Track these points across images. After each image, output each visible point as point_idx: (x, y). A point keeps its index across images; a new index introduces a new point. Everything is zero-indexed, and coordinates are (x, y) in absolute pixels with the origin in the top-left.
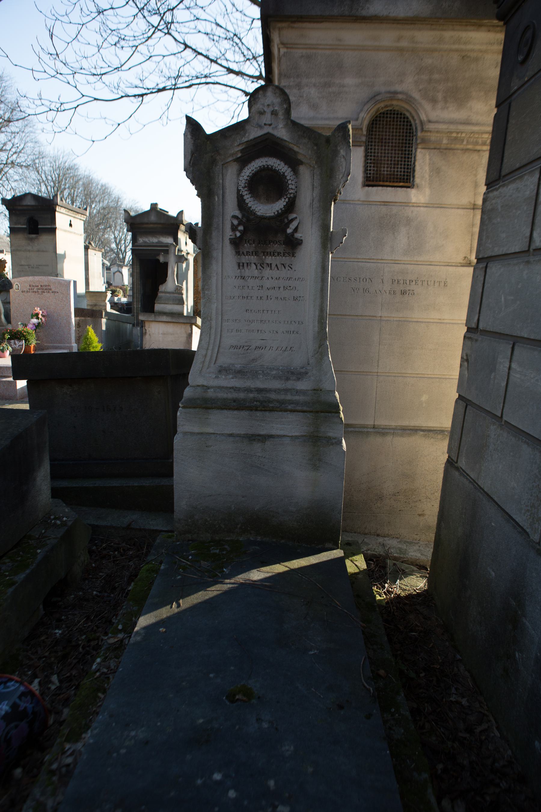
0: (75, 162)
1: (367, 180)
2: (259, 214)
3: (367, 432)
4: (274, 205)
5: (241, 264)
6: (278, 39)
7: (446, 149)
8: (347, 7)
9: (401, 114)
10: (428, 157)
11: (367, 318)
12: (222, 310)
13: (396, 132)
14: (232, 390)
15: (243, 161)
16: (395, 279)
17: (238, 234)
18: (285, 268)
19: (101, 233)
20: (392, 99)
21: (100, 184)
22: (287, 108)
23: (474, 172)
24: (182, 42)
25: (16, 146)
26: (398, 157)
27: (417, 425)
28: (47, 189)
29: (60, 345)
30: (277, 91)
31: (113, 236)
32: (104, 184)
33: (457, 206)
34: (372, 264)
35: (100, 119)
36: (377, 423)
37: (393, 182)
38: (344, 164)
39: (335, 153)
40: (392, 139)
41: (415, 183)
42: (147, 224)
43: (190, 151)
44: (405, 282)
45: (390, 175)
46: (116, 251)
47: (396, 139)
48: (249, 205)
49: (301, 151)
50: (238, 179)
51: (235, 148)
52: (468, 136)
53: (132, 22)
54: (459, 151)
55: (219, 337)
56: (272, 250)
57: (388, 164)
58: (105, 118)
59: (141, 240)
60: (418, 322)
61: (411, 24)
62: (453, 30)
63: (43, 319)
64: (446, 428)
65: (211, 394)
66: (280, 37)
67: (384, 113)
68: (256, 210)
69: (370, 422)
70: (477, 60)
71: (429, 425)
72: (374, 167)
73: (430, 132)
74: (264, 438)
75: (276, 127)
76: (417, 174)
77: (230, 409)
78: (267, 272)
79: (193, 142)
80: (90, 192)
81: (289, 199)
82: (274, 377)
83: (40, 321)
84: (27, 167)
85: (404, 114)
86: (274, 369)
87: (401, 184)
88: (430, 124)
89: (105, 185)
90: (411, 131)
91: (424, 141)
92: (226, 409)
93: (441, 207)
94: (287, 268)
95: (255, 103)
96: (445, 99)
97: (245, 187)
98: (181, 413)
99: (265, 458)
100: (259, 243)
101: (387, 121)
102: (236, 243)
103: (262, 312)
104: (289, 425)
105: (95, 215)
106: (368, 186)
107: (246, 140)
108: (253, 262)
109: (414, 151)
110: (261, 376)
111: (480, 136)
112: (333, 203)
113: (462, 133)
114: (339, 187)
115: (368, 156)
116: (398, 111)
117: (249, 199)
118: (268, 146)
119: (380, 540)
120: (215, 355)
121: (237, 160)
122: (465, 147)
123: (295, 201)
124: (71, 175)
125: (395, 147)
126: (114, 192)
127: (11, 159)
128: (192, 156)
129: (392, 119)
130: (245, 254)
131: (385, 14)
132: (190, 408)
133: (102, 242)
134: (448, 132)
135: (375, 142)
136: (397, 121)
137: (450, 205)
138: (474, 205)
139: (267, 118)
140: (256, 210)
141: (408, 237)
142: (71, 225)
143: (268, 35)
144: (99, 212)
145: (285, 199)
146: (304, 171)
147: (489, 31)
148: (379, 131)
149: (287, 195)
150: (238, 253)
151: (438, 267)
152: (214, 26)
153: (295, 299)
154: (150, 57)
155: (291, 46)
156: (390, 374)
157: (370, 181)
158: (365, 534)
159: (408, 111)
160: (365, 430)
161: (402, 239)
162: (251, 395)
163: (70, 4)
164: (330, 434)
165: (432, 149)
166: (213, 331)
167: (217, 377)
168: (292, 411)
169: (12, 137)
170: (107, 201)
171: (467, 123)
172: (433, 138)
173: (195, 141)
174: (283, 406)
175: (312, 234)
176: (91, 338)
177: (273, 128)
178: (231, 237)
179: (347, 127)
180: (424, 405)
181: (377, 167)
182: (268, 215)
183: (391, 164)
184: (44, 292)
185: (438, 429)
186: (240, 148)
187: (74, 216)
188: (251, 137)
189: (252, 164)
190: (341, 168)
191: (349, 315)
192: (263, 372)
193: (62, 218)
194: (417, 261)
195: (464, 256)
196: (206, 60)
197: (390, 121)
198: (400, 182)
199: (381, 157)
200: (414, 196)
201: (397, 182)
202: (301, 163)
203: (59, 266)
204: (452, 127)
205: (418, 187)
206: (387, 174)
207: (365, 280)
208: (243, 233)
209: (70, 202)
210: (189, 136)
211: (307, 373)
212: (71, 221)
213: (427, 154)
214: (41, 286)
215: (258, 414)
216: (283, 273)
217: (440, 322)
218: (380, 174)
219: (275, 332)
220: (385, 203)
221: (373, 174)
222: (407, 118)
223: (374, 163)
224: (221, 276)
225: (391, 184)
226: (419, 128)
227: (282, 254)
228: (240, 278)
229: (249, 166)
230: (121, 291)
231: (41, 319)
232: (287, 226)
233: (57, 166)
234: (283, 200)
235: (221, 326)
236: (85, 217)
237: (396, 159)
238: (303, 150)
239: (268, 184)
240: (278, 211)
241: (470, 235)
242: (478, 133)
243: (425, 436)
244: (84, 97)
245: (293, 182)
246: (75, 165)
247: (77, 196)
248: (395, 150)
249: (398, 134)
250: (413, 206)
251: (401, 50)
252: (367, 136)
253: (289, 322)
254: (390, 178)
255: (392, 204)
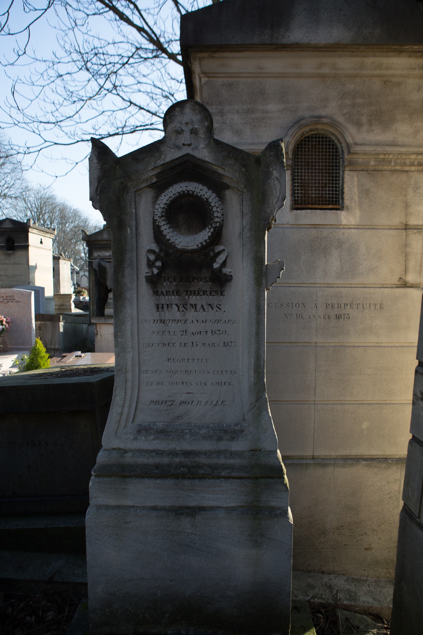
0: (53, 193)
1: (295, 204)
2: (179, 247)
3: (307, 464)
4: (198, 236)
5: (160, 306)
6: (199, 69)
7: (374, 171)
8: (267, 35)
9: (326, 138)
10: (356, 179)
11: (301, 344)
12: (139, 360)
13: (322, 155)
14: (154, 454)
15: (159, 188)
16: (329, 303)
17: (156, 271)
18: (212, 309)
19: (73, 246)
20: (316, 123)
21: (72, 209)
22: (208, 126)
23: (404, 193)
24: (128, 100)
25: (8, 183)
26: (326, 180)
27: (359, 454)
28: (32, 214)
29: (22, 347)
30: (197, 107)
31: (82, 248)
32: (75, 209)
33: (388, 227)
34: (304, 289)
35: (62, 159)
36: (316, 454)
37: (322, 204)
38: (278, 186)
39: (268, 175)
40: (319, 162)
41: (344, 205)
42: (101, 241)
43: (96, 177)
44: (339, 306)
45: (319, 197)
46: (85, 259)
47: (322, 162)
48: (168, 237)
49: (226, 174)
50: (154, 208)
51: (149, 172)
52: (395, 157)
53: (87, 85)
54: (387, 172)
55: (136, 391)
56: (196, 289)
57: (315, 187)
58: (66, 159)
59: (96, 254)
60: (354, 346)
61: (332, 51)
62: (374, 56)
63: (7, 326)
64: (389, 455)
65: (129, 459)
66: (200, 66)
67: (309, 137)
68: (176, 242)
69: (309, 453)
70: (399, 84)
71: (371, 454)
72: (301, 190)
73: (357, 154)
74: (193, 511)
75: (196, 147)
76: (346, 196)
77: (151, 477)
78: (191, 314)
79: (99, 167)
80: (65, 215)
81: (215, 228)
82: (204, 437)
83: (4, 327)
84: (16, 198)
85: (330, 138)
86: (203, 426)
87: (331, 206)
88: (357, 146)
89: (76, 210)
90: (338, 154)
91: (351, 163)
92: (148, 477)
93: (372, 229)
94: (215, 309)
95: (171, 122)
96: (370, 123)
97: (162, 216)
98: (93, 483)
99: (195, 534)
100: (181, 281)
101: (312, 145)
102: (153, 281)
103: (186, 361)
104: (223, 495)
105: (69, 232)
106: (297, 209)
107: (162, 163)
108: (174, 303)
109: (341, 173)
110: (188, 436)
111: (407, 157)
112: (267, 231)
113: (389, 154)
114: (273, 214)
115: (295, 179)
116: (323, 134)
117: (167, 231)
118: (188, 168)
119: (326, 579)
120: (133, 413)
121: (152, 186)
122: (393, 168)
123: (222, 230)
124: (51, 203)
125: (322, 169)
126: (83, 215)
127: (4, 193)
128: (99, 183)
129: (317, 143)
130: (165, 294)
131: (306, 42)
132: (104, 476)
133: (74, 253)
134: (376, 154)
135: (301, 165)
136: (322, 145)
137: (381, 226)
138: (406, 225)
139: (186, 138)
140: (176, 242)
141: (341, 260)
142: (41, 242)
143: (189, 68)
144: (71, 230)
145: (210, 229)
146: (232, 198)
147: (410, 56)
148: (305, 155)
149: (212, 224)
150: (156, 293)
151: (373, 289)
152: (153, 87)
153: (225, 345)
154: (103, 112)
155: (212, 75)
156: (328, 402)
157: (298, 204)
158: (309, 572)
159: (333, 134)
160: (304, 462)
161: (334, 262)
162: (177, 460)
163: (37, 74)
164: (274, 504)
165: (360, 171)
166: (129, 384)
167: (135, 439)
168: (226, 478)
169: (5, 176)
170: (77, 222)
171: (393, 144)
172: (360, 160)
173: (101, 166)
174: (215, 472)
175: (243, 269)
176: (38, 349)
177: (193, 149)
178: (148, 275)
179: (279, 145)
180: (365, 432)
181: (305, 190)
182: (190, 248)
183: (319, 187)
184: (9, 302)
185: (381, 457)
186: (155, 172)
187: (44, 235)
188: (168, 159)
189: (170, 190)
190: (274, 191)
191: (283, 343)
192: (190, 431)
193: (34, 238)
194: (351, 284)
195: (399, 277)
196: (148, 113)
197: (315, 145)
198: (329, 204)
199: (308, 180)
200: (345, 218)
201: (326, 204)
202: (228, 187)
203: (31, 276)
204: (379, 149)
205: (347, 208)
206: (315, 197)
207: (297, 305)
208: (162, 269)
209: (49, 223)
210: (95, 161)
211: (242, 431)
212: (41, 239)
213: (355, 176)
214: (6, 297)
215: (186, 482)
216: (211, 315)
217: (378, 346)
218: (308, 197)
219: (203, 384)
220: (315, 226)
221: (301, 197)
222: (333, 141)
223: (301, 186)
224: (136, 320)
225: (320, 207)
226: (346, 151)
227: (208, 293)
228: (159, 322)
229: (167, 192)
230: (86, 291)
231: (5, 325)
232: (214, 259)
233: (39, 197)
234: (207, 230)
235: (139, 378)
236: (54, 236)
237: (324, 181)
238: (229, 173)
239: (189, 212)
240: (202, 243)
241: (404, 256)
242: (405, 154)
243: (367, 465)
244: (46, 143)
245: (219, 210)
246: (53, 196)
247: (54, 218)
248: (322, 173)
249: (324, 157)
250: (344, 228)
251: (323, 76)
252: (293, 160)
253: (220, 372)
254: (319, 201)
255: (323, 226)
